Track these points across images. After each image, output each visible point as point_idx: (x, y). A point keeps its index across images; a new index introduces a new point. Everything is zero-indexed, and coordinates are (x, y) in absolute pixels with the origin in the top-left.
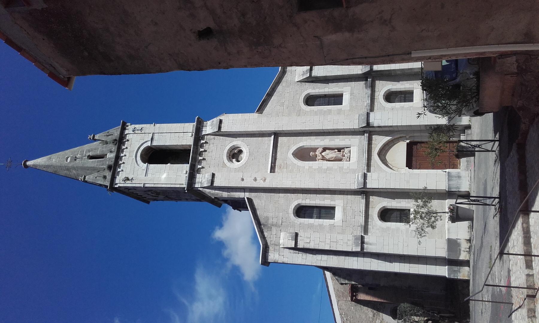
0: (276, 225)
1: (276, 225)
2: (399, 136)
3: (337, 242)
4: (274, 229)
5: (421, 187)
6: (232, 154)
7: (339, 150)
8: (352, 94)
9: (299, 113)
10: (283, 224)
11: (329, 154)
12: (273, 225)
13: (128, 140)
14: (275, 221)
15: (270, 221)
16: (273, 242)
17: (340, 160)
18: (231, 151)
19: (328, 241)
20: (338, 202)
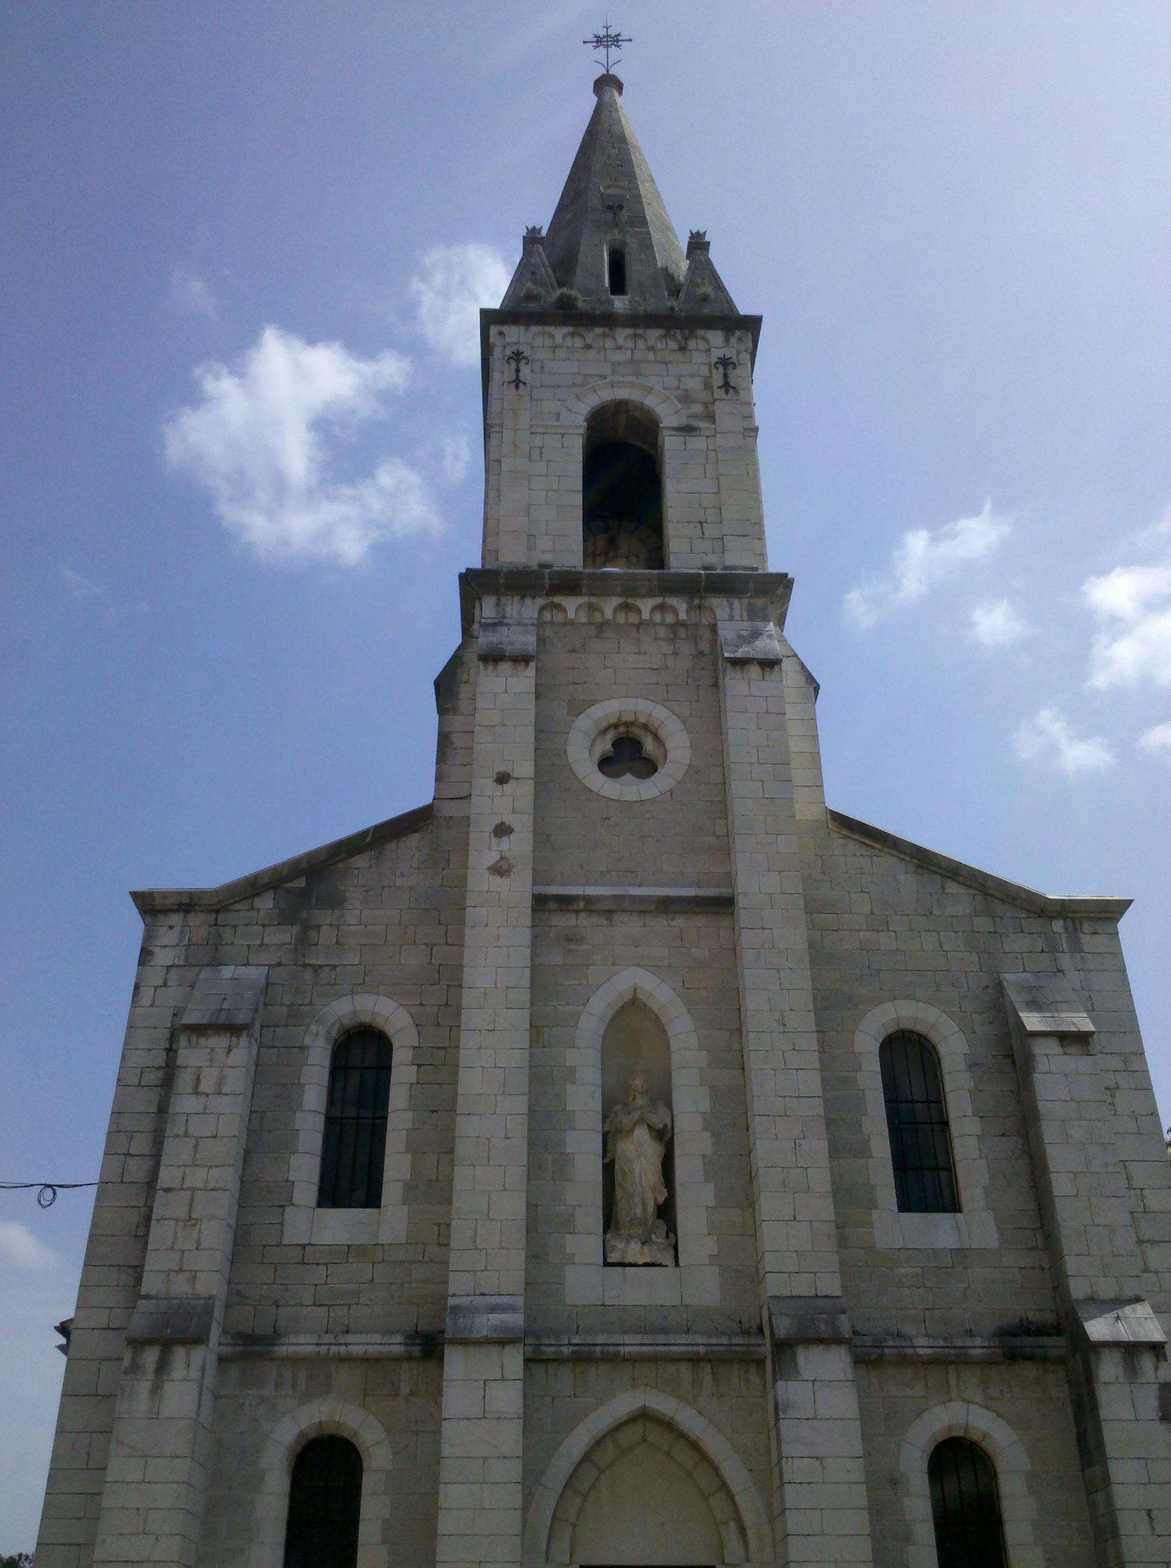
0: (303, 942)
1: (303, 942)
2: (748, 1520)
3: (190, 1221)
4: (286, 935)
5: (51, 1369)
6: (637, 732)
7: (666, 1212)
8: (961, 1254)
9: (832, 1009)
10: (308, 974)
11: (640, 1155)
12: (306, 928)
13: (683, 349)
14: (326, 935)
15: (325, 917)
16: (228, 934)
17: (610, 1221)
18: (645, 727)
19: (196, 1178)
20: (977, 1225)
